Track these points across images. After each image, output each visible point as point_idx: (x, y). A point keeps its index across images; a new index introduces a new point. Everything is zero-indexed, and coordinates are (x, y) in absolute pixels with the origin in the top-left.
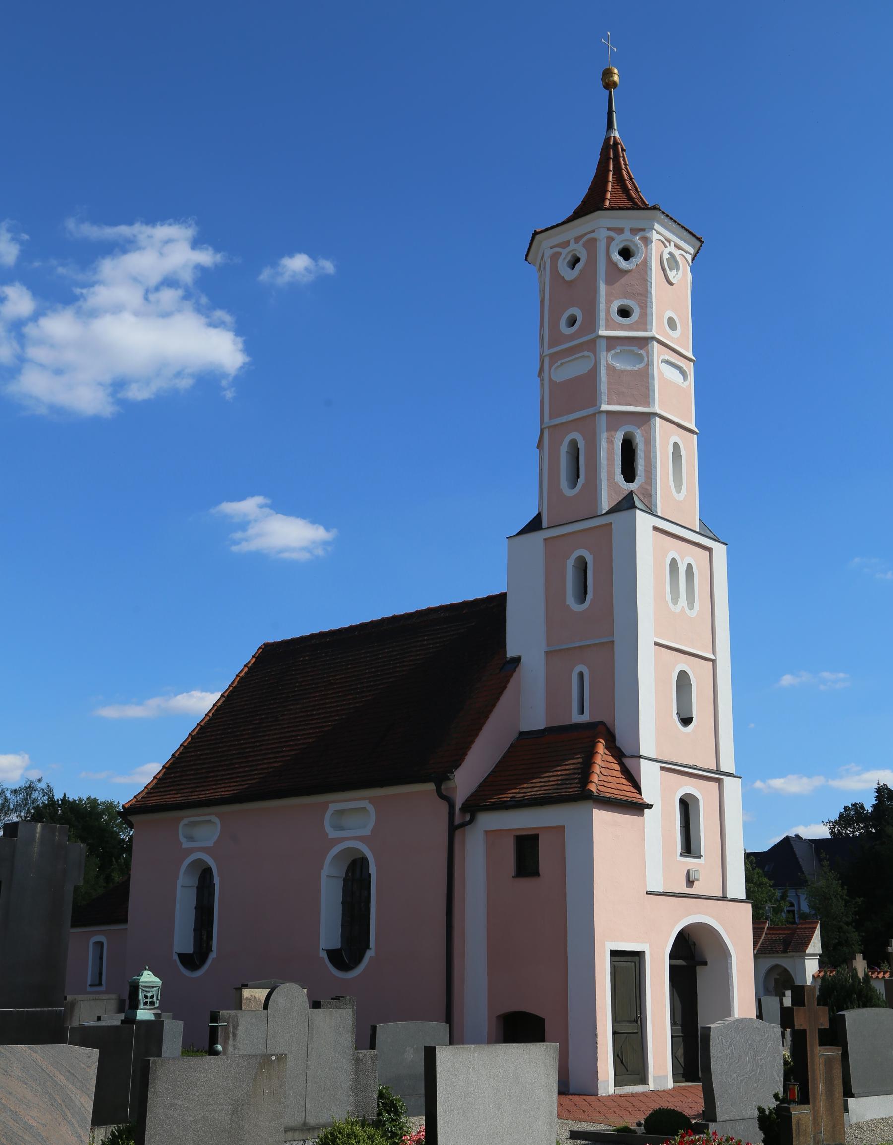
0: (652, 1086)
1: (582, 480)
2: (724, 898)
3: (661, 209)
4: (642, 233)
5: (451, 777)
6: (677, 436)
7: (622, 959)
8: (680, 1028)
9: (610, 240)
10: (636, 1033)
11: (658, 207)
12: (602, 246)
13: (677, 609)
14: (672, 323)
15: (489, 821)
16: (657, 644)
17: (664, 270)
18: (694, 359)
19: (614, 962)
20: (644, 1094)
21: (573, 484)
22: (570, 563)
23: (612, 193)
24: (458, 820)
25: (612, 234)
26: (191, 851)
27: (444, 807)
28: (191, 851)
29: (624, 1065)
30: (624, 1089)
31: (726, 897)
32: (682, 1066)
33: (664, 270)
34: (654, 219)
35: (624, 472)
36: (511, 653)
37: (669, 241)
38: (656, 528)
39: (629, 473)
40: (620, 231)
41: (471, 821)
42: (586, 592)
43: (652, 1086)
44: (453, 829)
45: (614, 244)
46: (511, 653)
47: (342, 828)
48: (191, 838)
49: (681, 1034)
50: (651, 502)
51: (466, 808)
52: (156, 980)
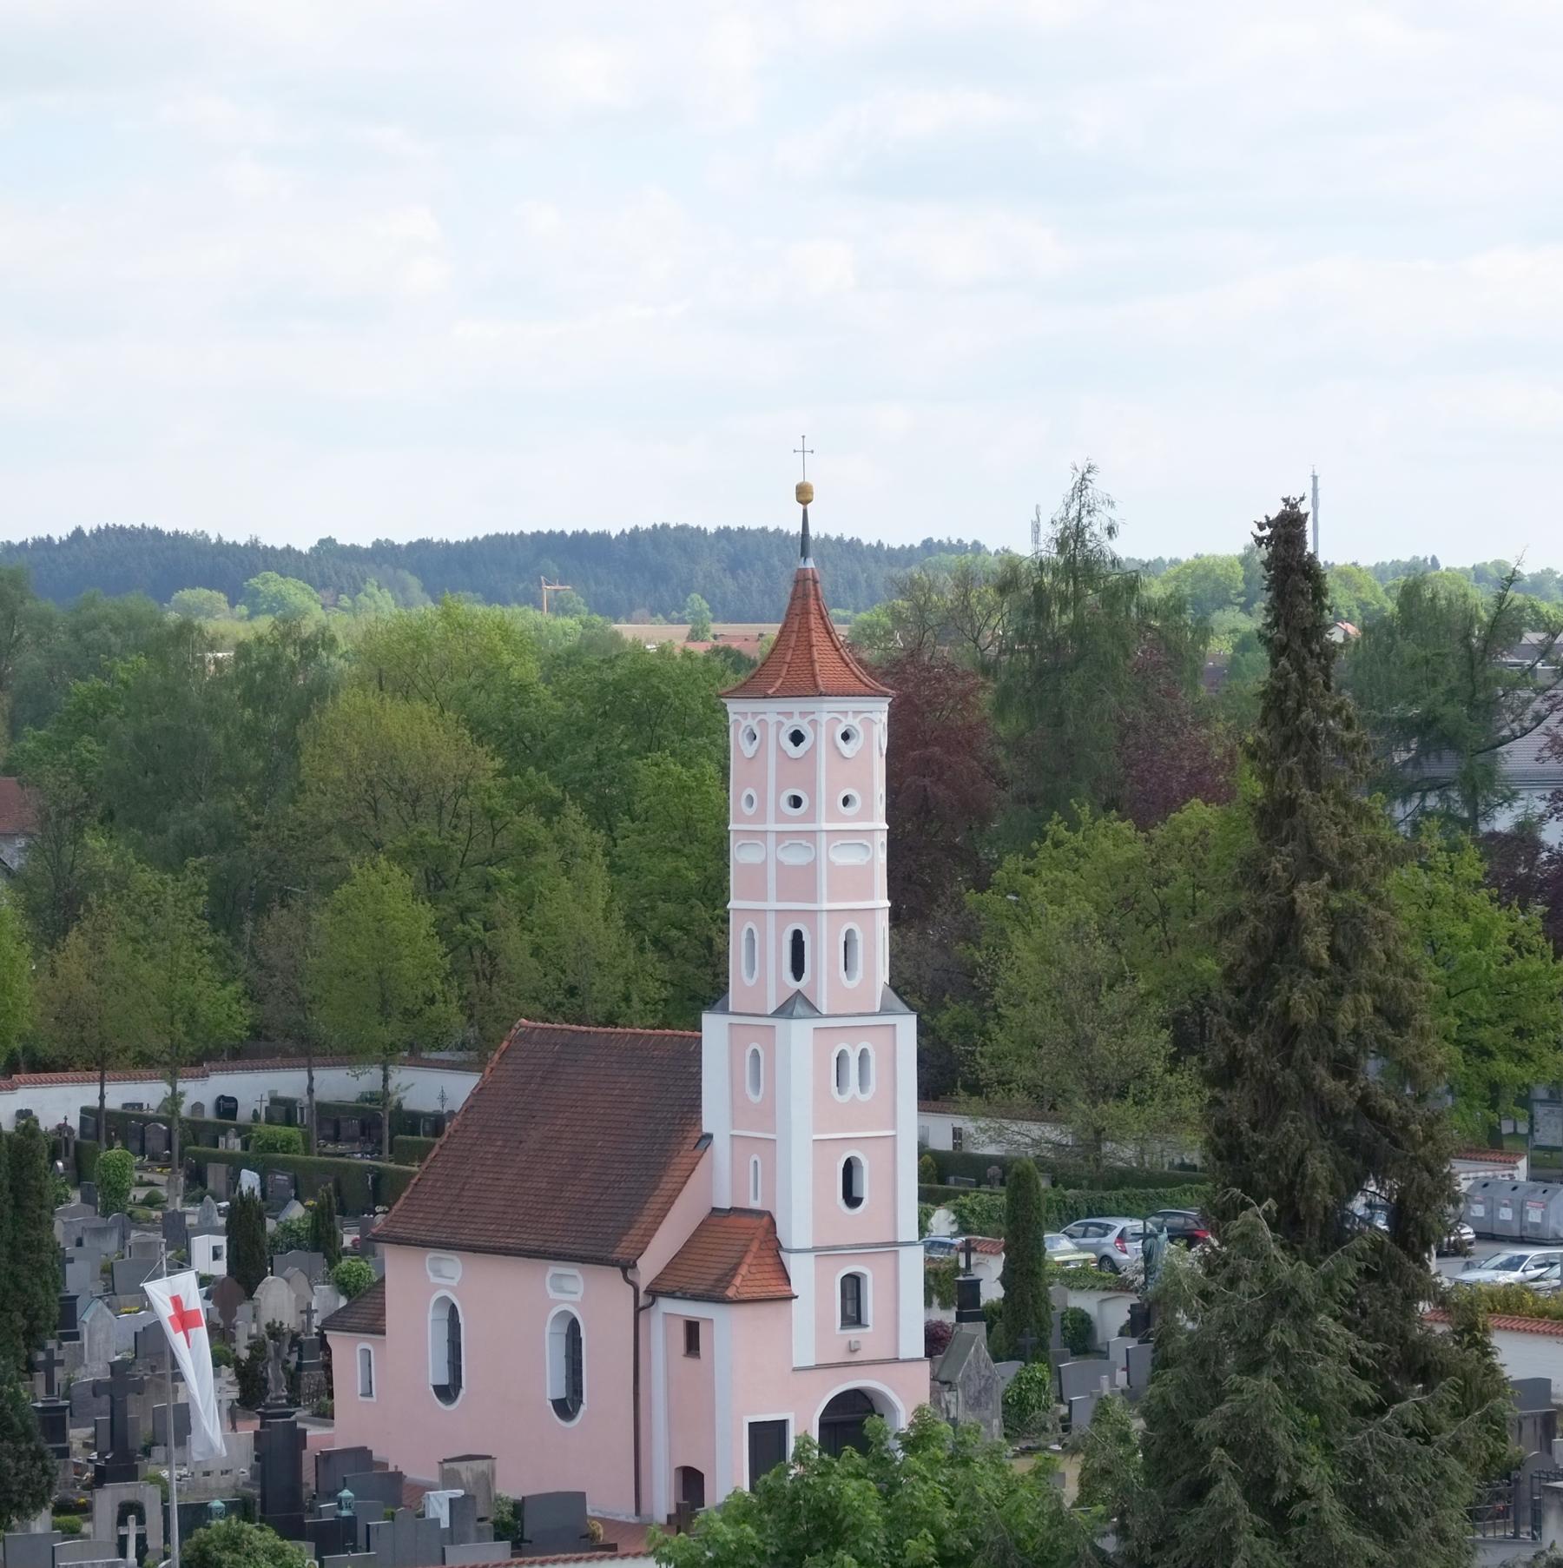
1: (756, 973)
2: (896, 1360)
4: (811, 717)
5: (1377, 607)
9: (780, 724)
12: (772, 731)
13: (845, 1098)
15: (665, 1305)
21: (751, 974)
22: (748, 1053)
24: (641, 1303)
25: (781, 718)
26: (439, 1286)
27: (631, 1289)
28: (438, 1287)
36: (706, 1129)
39: (798, 969)
40: (790, 714)
41: (652, 1304)
42: (759, 1085)
44: (638, 1310)
45: (784, 729)
46: (706, 1129)
47: (562, 1290)
48: (438, 1273)
51: (647, 1292)
52: (351, 1494)
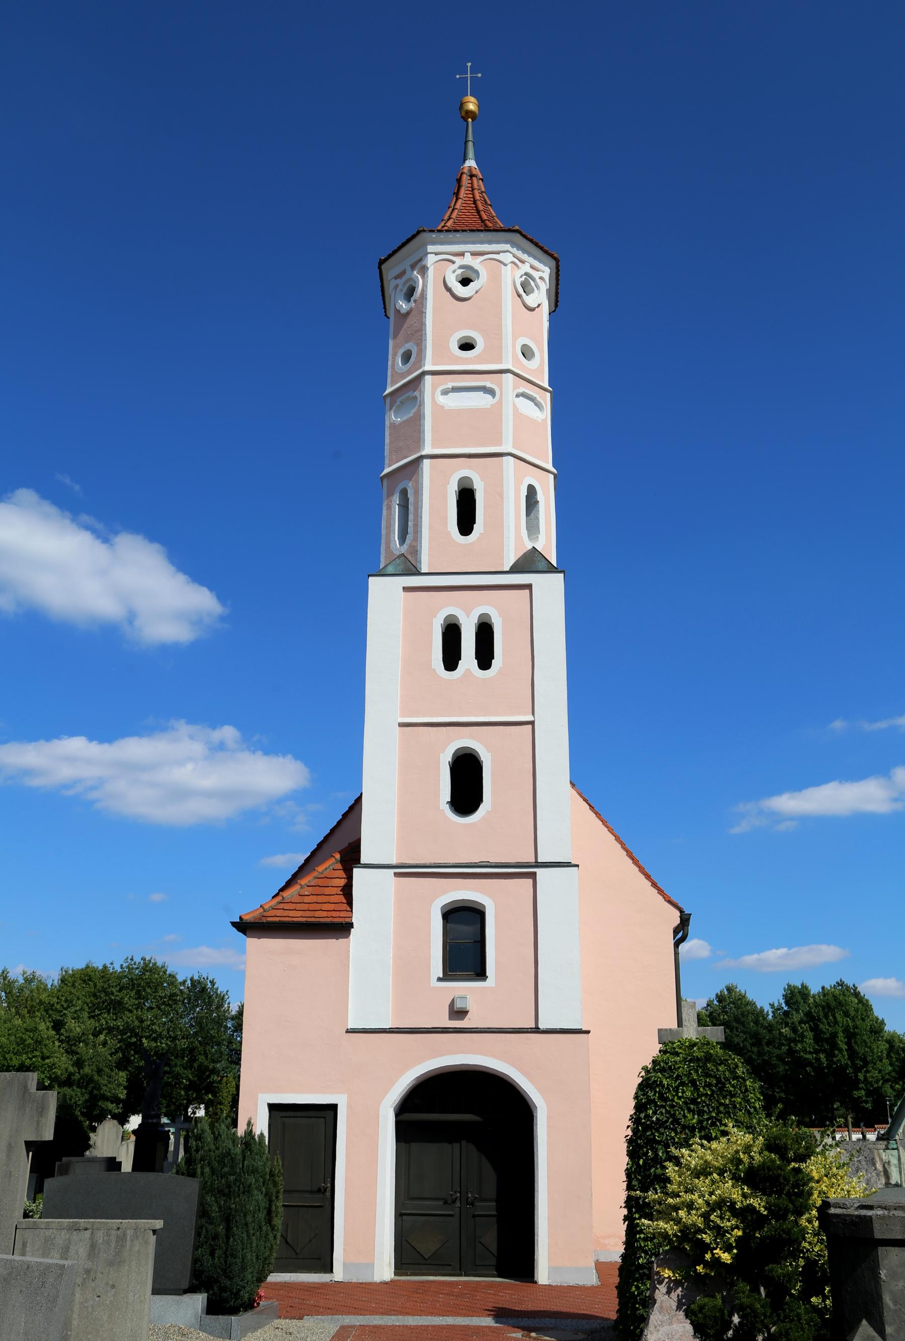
0: (338, 1274)
2: (536, 1030)
3: (425, 229)
6: (532, 478)
7: (299, 1114)
8: (495, 1204)
10: (452, 1216)
11: (421, 229)
14: (527, 353)
16: (402, 725)
17: (519, 296)
18: (551, 390)
19: (284, 1119)
20: (324, 1285)
23: (456, 221)
29: (291, 1246)
30: (279, 1276)
31: (539, 1028)
32: (493, 1255)
33: (519, 296)
34: (425, 245)
35: (528, 528)
37: (523, 262)
38: (406, 589)
43: (338, 1274)
49: (495, 1213)
50: (416, 559)
